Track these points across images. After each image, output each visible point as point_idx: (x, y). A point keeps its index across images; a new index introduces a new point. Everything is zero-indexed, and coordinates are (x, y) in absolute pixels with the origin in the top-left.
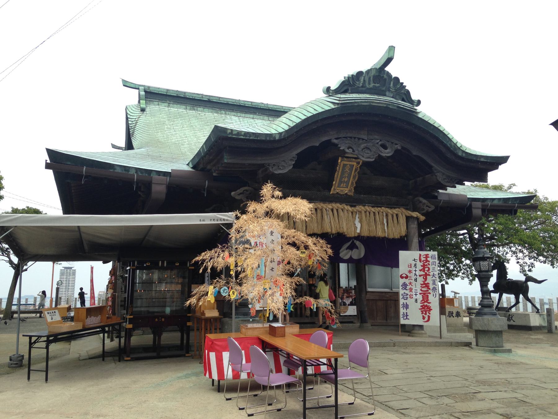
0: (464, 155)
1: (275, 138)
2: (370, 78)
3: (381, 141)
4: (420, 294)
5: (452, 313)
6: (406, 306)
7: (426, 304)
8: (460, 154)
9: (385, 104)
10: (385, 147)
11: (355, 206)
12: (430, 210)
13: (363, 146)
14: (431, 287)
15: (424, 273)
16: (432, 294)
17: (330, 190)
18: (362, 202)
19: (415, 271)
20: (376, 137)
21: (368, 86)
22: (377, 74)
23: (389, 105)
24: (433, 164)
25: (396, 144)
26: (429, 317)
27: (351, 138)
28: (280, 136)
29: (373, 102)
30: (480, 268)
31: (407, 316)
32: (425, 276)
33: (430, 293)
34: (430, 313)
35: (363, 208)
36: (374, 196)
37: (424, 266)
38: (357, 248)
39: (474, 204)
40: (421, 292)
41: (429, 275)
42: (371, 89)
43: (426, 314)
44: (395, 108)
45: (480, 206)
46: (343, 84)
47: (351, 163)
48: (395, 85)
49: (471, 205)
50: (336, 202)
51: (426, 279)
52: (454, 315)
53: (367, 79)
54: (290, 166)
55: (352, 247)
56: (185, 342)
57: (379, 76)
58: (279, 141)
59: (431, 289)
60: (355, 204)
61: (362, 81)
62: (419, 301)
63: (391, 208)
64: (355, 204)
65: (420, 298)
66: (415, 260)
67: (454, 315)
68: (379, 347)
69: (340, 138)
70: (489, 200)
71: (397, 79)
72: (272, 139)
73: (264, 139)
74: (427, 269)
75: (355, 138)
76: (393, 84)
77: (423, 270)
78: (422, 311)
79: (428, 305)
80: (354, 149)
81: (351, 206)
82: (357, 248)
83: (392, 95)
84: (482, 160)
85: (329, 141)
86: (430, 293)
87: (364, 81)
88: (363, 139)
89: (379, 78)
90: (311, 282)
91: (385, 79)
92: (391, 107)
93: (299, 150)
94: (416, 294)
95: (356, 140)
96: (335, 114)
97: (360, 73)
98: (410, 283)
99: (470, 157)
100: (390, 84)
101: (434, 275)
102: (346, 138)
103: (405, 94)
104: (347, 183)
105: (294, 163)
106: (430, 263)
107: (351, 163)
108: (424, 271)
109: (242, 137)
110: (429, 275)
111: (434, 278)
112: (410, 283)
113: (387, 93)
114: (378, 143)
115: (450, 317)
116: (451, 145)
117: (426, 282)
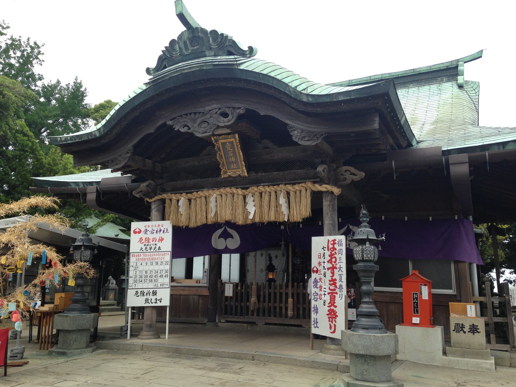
0: (310, 99)
1: (95, 135)
2: (185, 43)
3: (220, 109)
4: (329, 293)
5: (463, 326)
6: (316, 311)
7: (332, 307)
8: (305, 99)
9: (198, 67)
10: (225, 115)
11: (247, 188)
12: (356, 178)
13: (199, 121)
14: (338, 285)
15: (331, 266)
16: (338, 295)
17: (220, 175)
18: (257, 182)
19: (324, 262)
20: (214, 106)
21: (186, 53)
22: (191, 35)
23: (203, 66)
24: (287, 122)
25: (239, 108)
26: (335, 326)
27: (186, 115)
28: (100, 133)
29: (184, 70)
30: (363, 256)
31: (317, 323)
32: (333, 268)
33: (336, 293)
34: (335, 322)
35: (256, 189)
36: (275, 173)
37: (331, 255)
38: (232, 237)
39: (452, 158)
40: (330, 291)
41: (336, 268)
42: (190, 54)
43: (332, 322)
44: (211, 67)
45: (467, 160)
46: (161, 60)
47: (229, 140)
48: (215, 40)
49: (447, 161)
50: (226, 186)
51: (333, 273)
52: (466, 329)
53: (182, 45)
54: (125, 159)
55: (226, 235)
56: (47, 327)
57: (194, 36)
58: (102, 137)
59: (338, 287)
60: (248, 186)
61: (178, 49)
62: (327, 304)
63: (294, 184)
64: (248, 186)
65: (327, 298)
66: (323, 248)
67: (466, 329)
68: (234, 358)
69: (176, 118)
70: (494, 147)
71: (214, 32)
72: (93, 137)
73: (86, 139)
74: (334, 260)
75: (190, 114)
76: (212, 39)
77: (330, 261)
78: (329, 318)
79: (335, 309)
80: (190, 126)
81: (243, 189)
82: (232, 237)
83: (213, 54)
84: (341, 98)
85: (165, 124)
86: (336, 293)
87: (180, 48)
88: (200, 113)
89: (195, 40)
90: (271, 277)
91: (202, 38)
92: (204, 68)
93: (135, 142)
94: (325, 294)
95: (193, 115)
96: (152, 94)
97: (173, 42)
98: (320, 279)
99: (320, 100)
100: (209, 41)
101: (340, 268)
102: (181, 116)
103: (230, 45)
104: (236, 162)
105: (129, 155)
106: (337, 252)
107: (229, 140)
108: (331, 263)
109: (69, 142)
110: (336, 268)
111: (340, 272)
112: (320, 279)
113: (207, 53)
114: (216, 113)
115: (458, 332)
116: (289, 91)
117: (334, 278)
